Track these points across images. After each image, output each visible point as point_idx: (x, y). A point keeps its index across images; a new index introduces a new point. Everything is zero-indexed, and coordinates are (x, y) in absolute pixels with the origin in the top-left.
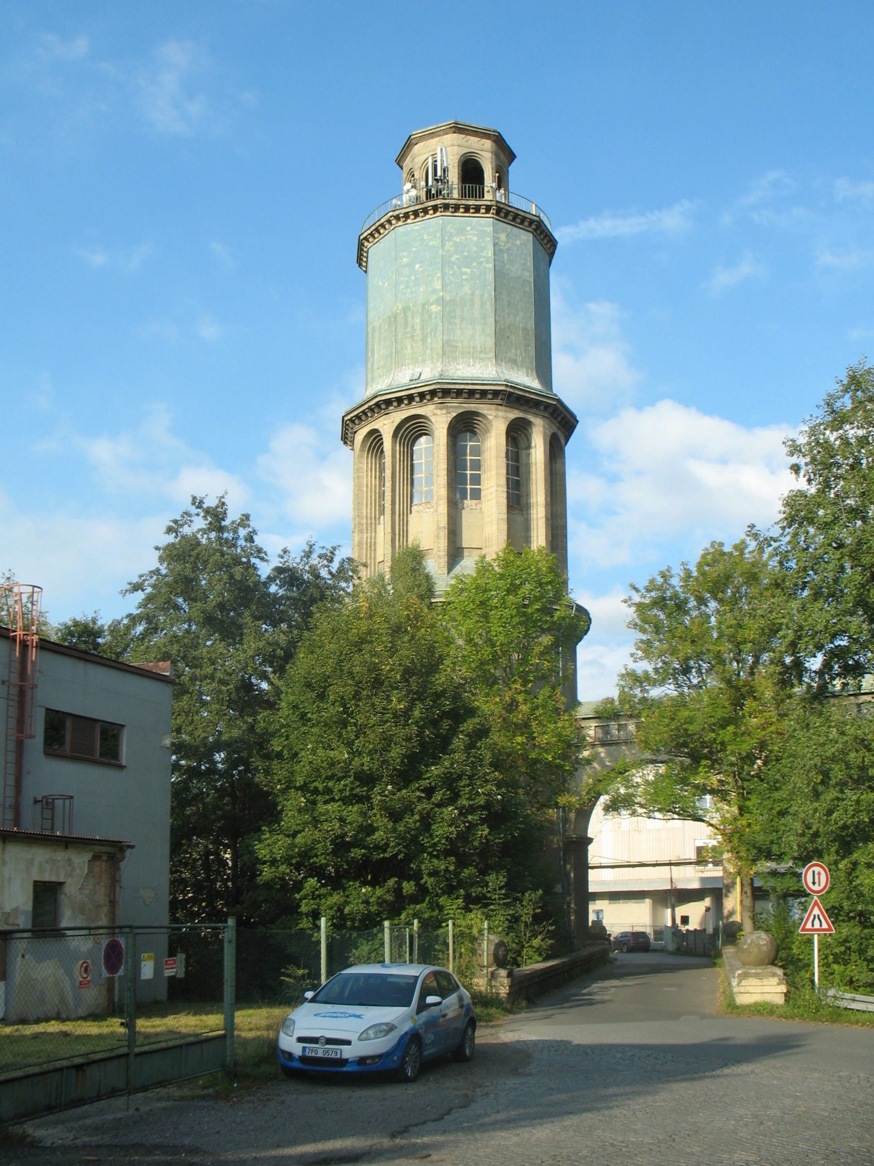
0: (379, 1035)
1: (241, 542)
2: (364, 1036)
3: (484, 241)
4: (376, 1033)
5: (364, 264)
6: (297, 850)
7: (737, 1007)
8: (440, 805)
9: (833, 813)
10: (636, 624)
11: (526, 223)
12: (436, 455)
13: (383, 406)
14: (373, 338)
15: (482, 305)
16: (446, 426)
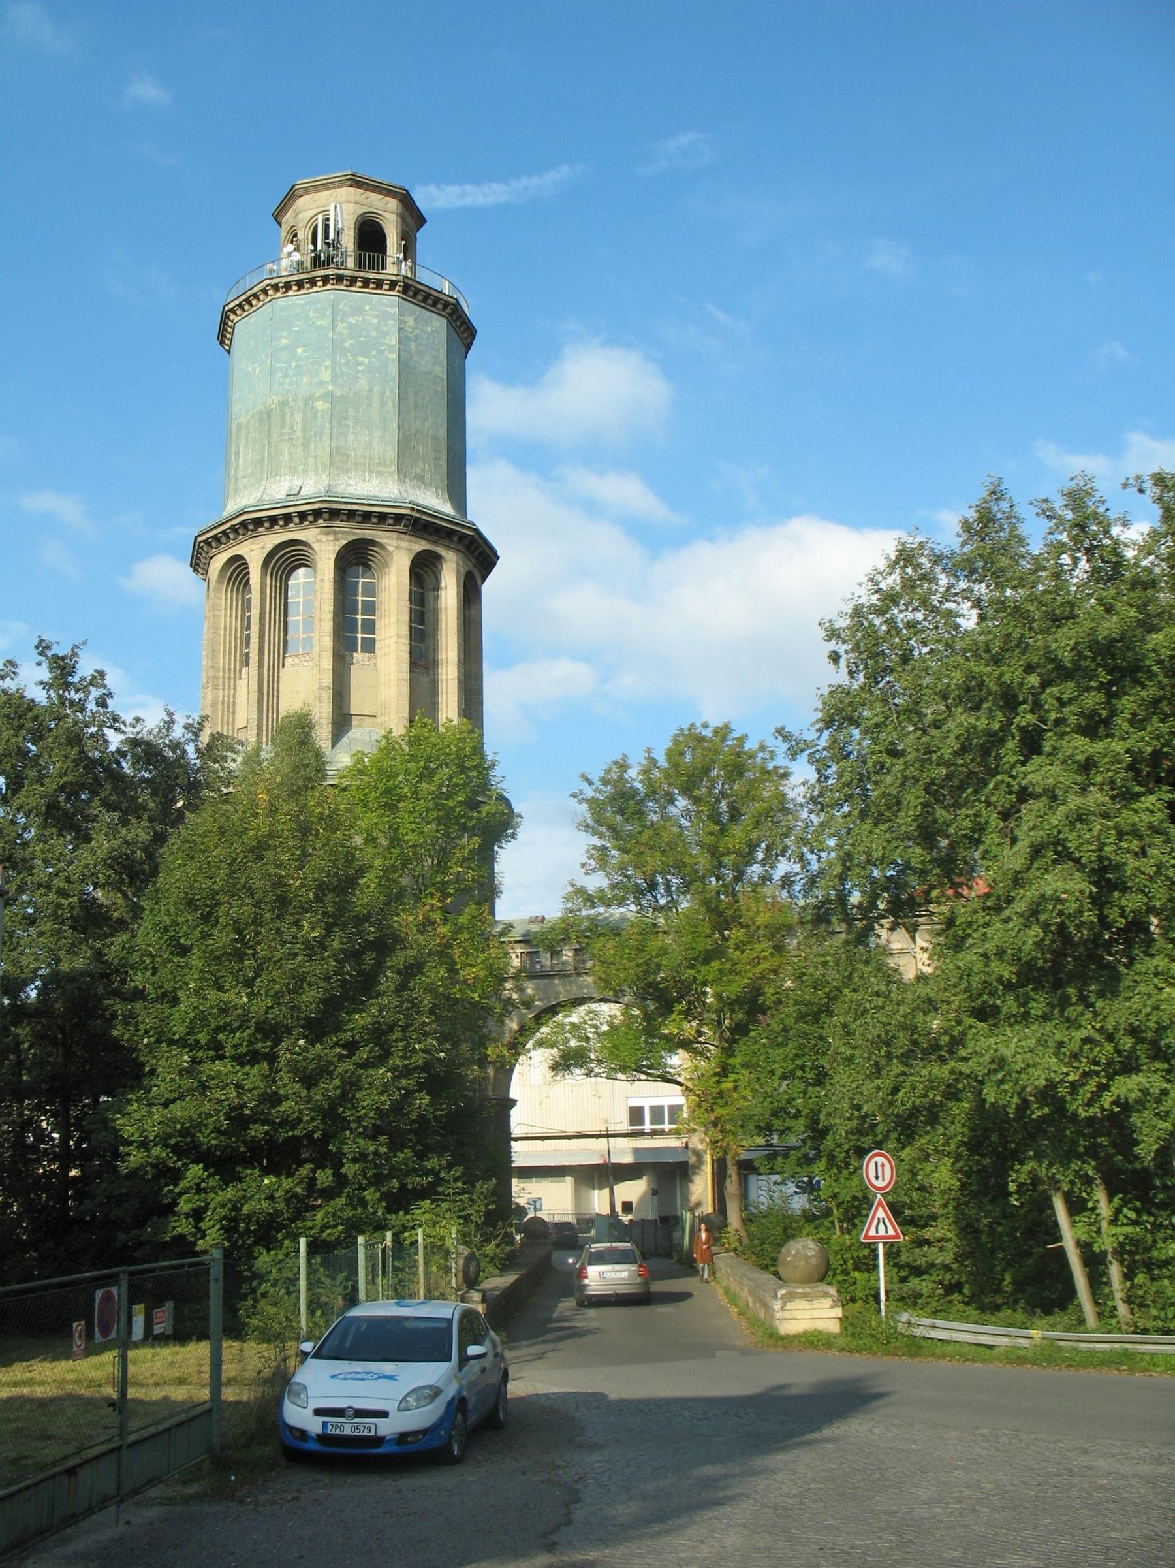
0: (422, 1403)
1: (91, 706)
2: (403, 1405)
3: (386, 325)
4: (418, 1400)
5: (227, 342)
6: (179, 1126)
7: (782, 1338)
8: (365, 1065)
9: (899, 1090)
10: (588, 826)
11: (440, 306)
12: (318, 592)
13: (251, 527)
14: (238, 437)
15: (383, 403)
16: (333, 557)
